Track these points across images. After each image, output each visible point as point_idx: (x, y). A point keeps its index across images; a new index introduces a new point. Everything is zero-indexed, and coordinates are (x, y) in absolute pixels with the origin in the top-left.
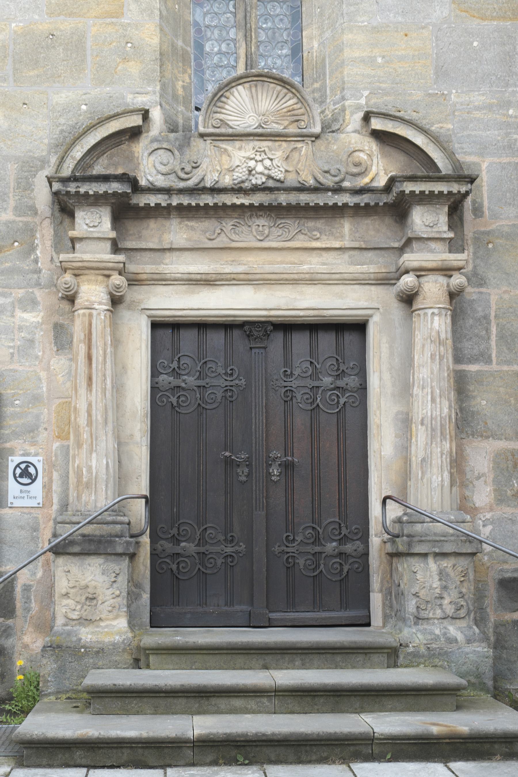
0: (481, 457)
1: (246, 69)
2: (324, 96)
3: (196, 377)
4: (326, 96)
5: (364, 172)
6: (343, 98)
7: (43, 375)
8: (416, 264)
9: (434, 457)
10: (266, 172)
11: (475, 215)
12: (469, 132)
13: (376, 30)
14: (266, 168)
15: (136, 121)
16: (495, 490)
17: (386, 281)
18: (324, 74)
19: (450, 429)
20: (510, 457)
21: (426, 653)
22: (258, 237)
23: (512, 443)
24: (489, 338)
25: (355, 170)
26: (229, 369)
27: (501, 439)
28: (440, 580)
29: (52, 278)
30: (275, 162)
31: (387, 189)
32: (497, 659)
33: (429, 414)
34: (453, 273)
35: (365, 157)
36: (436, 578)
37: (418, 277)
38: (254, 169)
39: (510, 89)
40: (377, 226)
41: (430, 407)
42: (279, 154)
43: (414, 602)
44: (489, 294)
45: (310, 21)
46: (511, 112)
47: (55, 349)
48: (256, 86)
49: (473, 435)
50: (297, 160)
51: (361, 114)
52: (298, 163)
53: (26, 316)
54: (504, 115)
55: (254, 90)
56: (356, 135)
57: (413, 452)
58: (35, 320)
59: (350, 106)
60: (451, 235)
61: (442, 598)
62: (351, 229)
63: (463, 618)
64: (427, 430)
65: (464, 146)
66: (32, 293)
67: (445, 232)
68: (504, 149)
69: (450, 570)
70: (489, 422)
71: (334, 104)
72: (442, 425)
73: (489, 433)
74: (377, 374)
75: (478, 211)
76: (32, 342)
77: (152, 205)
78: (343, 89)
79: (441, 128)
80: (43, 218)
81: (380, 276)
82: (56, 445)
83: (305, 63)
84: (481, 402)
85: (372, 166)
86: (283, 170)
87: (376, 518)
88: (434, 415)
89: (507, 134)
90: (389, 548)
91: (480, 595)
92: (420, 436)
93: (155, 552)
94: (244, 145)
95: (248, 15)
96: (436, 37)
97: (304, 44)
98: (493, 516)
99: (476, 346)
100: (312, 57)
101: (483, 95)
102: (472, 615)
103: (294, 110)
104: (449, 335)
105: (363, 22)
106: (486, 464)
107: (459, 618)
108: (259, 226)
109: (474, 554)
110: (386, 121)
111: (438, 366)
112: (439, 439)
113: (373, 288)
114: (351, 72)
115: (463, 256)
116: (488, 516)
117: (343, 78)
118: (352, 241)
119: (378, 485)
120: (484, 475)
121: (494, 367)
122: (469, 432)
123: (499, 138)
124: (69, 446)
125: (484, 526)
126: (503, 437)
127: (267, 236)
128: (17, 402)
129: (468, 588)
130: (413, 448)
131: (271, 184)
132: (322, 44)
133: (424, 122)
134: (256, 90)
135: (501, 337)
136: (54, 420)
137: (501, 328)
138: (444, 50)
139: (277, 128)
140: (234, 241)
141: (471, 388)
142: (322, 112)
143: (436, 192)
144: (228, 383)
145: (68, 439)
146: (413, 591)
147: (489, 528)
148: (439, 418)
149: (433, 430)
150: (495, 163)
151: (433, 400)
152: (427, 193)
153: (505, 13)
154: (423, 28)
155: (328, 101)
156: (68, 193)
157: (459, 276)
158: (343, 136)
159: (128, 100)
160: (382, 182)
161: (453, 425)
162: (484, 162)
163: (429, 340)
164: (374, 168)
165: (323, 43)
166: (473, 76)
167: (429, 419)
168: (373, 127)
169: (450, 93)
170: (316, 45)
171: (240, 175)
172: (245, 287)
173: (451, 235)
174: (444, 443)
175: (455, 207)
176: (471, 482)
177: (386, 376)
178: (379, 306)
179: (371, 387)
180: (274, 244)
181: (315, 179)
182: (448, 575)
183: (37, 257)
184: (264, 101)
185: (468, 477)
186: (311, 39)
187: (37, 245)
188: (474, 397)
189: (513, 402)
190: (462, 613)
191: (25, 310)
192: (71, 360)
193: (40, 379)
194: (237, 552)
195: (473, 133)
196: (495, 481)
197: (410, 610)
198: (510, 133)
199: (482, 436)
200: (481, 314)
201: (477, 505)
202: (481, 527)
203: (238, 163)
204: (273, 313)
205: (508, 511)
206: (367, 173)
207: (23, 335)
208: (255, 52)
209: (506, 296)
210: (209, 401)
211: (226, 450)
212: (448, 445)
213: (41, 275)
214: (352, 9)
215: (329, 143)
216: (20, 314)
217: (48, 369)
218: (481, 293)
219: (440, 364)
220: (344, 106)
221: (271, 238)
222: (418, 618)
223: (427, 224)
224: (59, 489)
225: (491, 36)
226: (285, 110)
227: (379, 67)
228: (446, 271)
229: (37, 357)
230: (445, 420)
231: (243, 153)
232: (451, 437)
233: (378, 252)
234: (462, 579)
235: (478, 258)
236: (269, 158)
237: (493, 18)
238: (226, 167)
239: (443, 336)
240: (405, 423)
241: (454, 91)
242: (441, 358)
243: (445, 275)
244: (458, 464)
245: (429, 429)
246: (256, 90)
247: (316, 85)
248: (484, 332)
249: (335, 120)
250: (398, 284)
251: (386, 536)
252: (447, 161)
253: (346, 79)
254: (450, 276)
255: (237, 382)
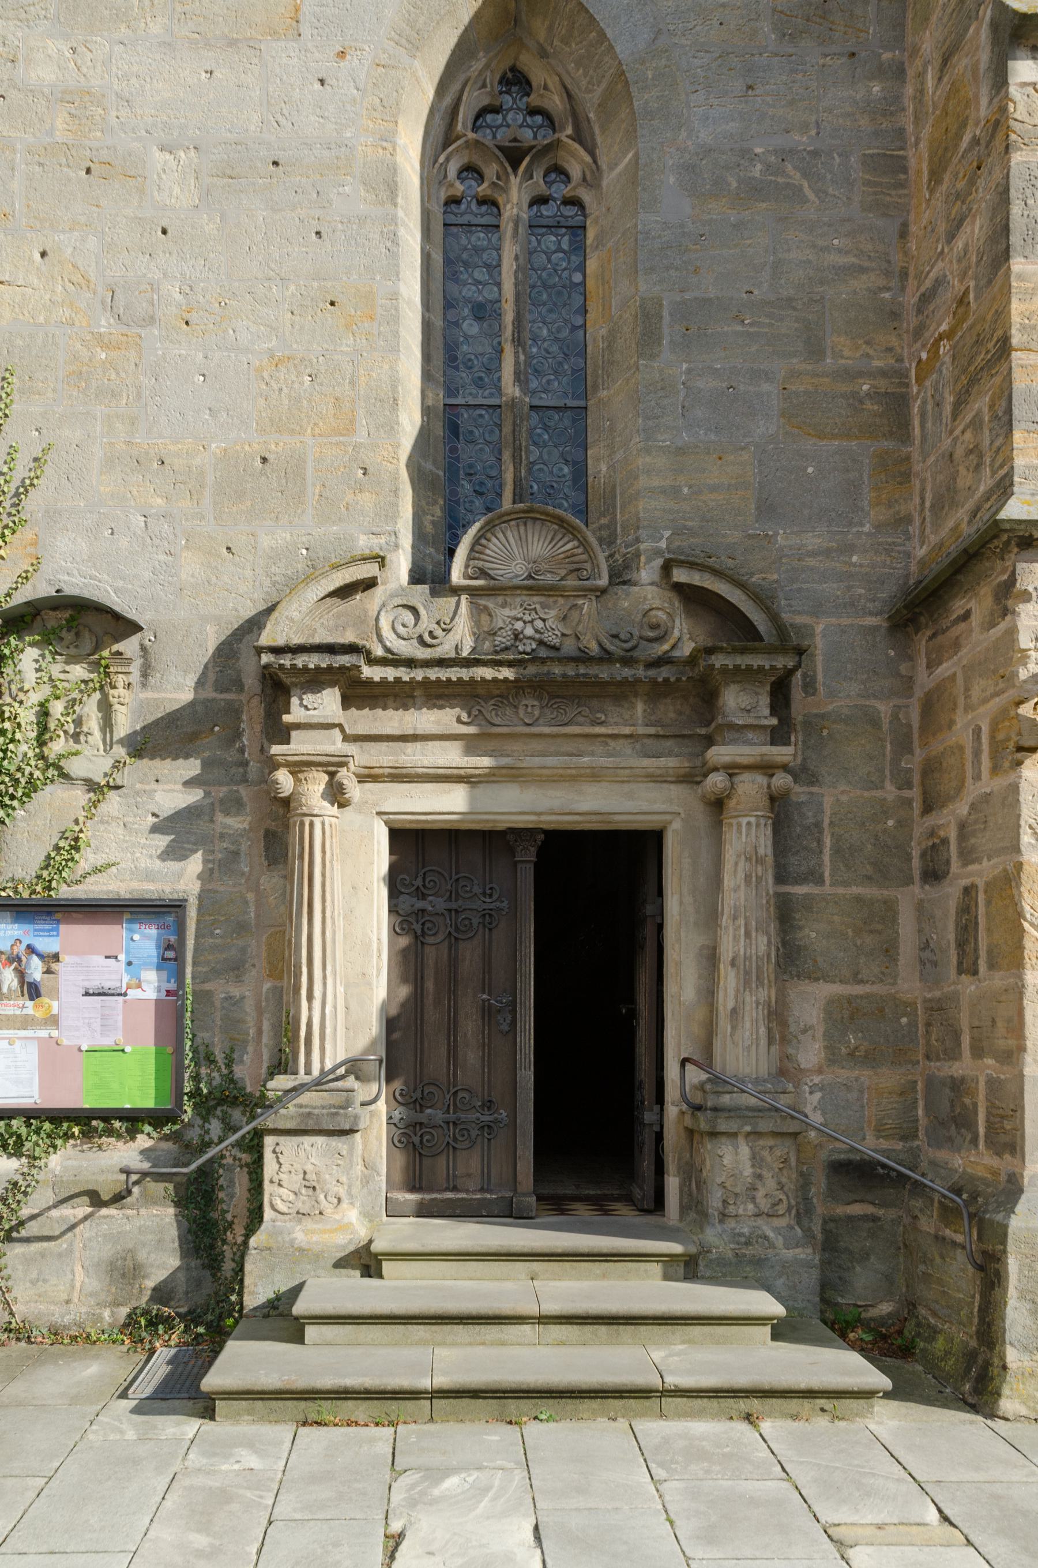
0: (811, 1003)
1: (514, 502)
2: (613, 535)
3: (445, 898)
4: (616, 535)
5: (663, 637)
6: (638, 540)
7: (250, 896)
8: (727, 759)
9: (747, 1008)
10: (537, 636)
11: (806, 692)
12: (799, 585)
13: (681, 451)
14: (537, 631)
15: (368, 570)
16: (826, 1047)
17: (692, 778)
18: (614, 507)
19: (769, 970)
20: (846, 1005)
21: (734, 1260)
22: (527, 721)
23: (849, 987)
24: (821, 852)
25: (651, 634)
26: (488, 887)
27: (835, 982)
28: (753, 1166)
29: (263, 772)
30: (549, 623)
31: (692, 660)
32: (825, 1264)
33: (742, 952)
34: (776, 771)
35: (664, 617)
36: (748, 1164)
37: (731, 775)
38: (522, 632)
39: (855, 530)
40: (679, 707)
41: (742, 943)
42: (553, 613)
43: (719, 1194)
44: (823, 795)
45: (597, 437)
46: (855, 559)
47: (266, 863)
48: (525, 524)
49: (799, 977)
50: (577, 620)
51: (659, 562)
52: (578, 625)
53: (230, 821)
54: (846, 563)
55: (522, 529)
56: (654, 588)
57: (721, 1000)
58: (241, 826)
59: (646, 550)
60: (774, 721)
61: (755, 1189)
62: (645, 711)
63: (782, 1215)
64: (738, 972)
65: (793, 603)
66: (237, 791)
67: (766, 718)
68: (845, 607)
69: (765, 1153)
70: (820, 959)
71: (626, 547)
72: (758, 967)
73: (819, 974)
74: (676, 897)
75: (809, 686)
76: (236, 854)
77: (391, 679)
78: (638, 528)
79: (764, 579)
80: (252, 694)
81: (682, 771)
82: (267, 986)
83: (590, 491)
84: (811, 933)
85: (673, 628)
86: (559, 634)
87: (673, 1080)
88: (748, 954)
89: (849, 588)
90: (688, 1121)
91: (804, 1182)
92: (729, 980)
93: (392, 1121)
94: (508, 600)
95: (517, 429)
96: (759, 461)
97: (589, 467)
98: (822, 1080)
99: (804, 862)
100: (599, 483)
101: (819, 536)
102: (794, 1212)
103: (574, 555)
104: (770, 851)
105: (664, 441)
106: (815, 1014)
107: (778, 1216)
108: (527, 706)
109: (795, 1135)
110: (692, 572)
111: (754, 892)
112: (754, 985)
113: (672, 787)
114: (647, 507)
115: (789, 750)
116: (817, 1079)
117: (638, 513)
118: (647, 725)
119: (678, 1040)
120: (812, 1027)
121: (827, 889)
122: (794, 973)
123: (839, 593)
124: (282, 987)
125: (811, 1093)
126: (837, 979)
127: (537, 719)
128: (218, 931)
129: (790, 1179)
130: (721, 994)
131: (543, 653)
132: (611, 467)
133: (743, 571)
134: (526, 531)
135: (837, 851)
136: (264, 955)
137: (837, 839)
138: (769, 477)
139: (549, 579)
140: (495, 725)
141: (797, 916)
142: (611, 556)
143: (755, 667)
144: (486, 906)
145: (281, 978)
146: (719, 1180)
147: (818, 1095)
148: (754, 958)
149: (747, 973)
150: (832, 625)
151: (748, 934)
152: (743, 667)
153: (850, 429)
154: (743, 449)
155: (619, 542)
156: (282, 667)
157: (783, 775)
158: (636, 589)
159: (361, 542)
160: (687, 649)
161: (772, 967)
162: (818, 623)
163: (743, 857)
164: (676, 633)
165: (613, 466)
166: (806, 512)
167: (742, 960)
168: (675, 579)
169: (777, 534)
170: (604, 468)
171: (504, 640)
172: (509, 785)
173: (774, 721)
174: (761, 989)
175: (780, 693)
176: (795, 1037)
177: (688, 899)
178: (681, 810)
179: (669, 915)
180: (547, 730)
181: (600, 645)
182: (762, 1160)
183: (244, 746)
184: (535, 543)
185: (792, 1029)
186: (598, 460)
187: (244, 730)
188: (801, 928)
189: (850, 934)
190: (781, 1209)
191: (227, 814)
192: (285, 877)
193: (247, 902)
194: (496, 1121)
195: (804, 586)
196: (827, 1035)
197: (715, 1204)
198: (852, 587)
199: (810, 978)
200: (811, 820)
201: (802, 1066)
202: (807, 1095)
203: (501, 624)
204: (543, 818)
205: (845, 1074)
206: (667, 637)
207: (225, 845)
208: (525, 477)
209: (844, 798)
210: (463, 929)
211: (484, 992)
212: (766, 992)
213: (249, 769)
214: (650, 423)
215: (618, 599)
216: (220, 818)
217: (257, 890)
218: (811, 793)
219: (757, 889)
220: (638, 550)
221: (541, 721)
222: (724, 1215)
223: (743, 707)
224: (271, 1043)
225: (831, 460)
226: (562, 556)
227: (684, 500)
228: (767, 768)
229: (243, 874)
230: (762, 959)
231: (507, 612)
232: (769, 981)
233: (680, 740)
234: (782, 1165)
235: (808, 748)
236: (540, 618)
237: (834, 437)
238: (486, 629)
239: (761, 851)
240: (711, 958)
241: (781, 532)
242: (759, 879)
243: (765, 774)
244: (777, 1017)
245: (742, 972)
246: (526, 531)
247: (604, 521)
248: (815, 844)
249: (627, 567)
250: (704, 783)
251: (685, 1107)
252: (770, 623)
253: (641, 515)
254: (772, 775)
255: (498, 904)
